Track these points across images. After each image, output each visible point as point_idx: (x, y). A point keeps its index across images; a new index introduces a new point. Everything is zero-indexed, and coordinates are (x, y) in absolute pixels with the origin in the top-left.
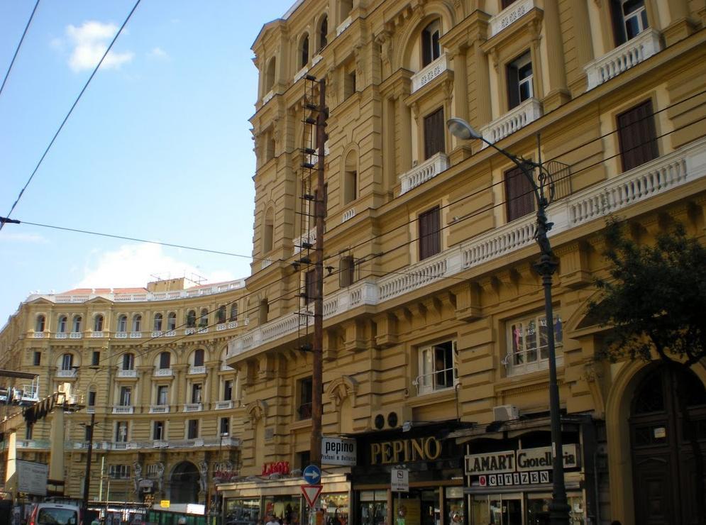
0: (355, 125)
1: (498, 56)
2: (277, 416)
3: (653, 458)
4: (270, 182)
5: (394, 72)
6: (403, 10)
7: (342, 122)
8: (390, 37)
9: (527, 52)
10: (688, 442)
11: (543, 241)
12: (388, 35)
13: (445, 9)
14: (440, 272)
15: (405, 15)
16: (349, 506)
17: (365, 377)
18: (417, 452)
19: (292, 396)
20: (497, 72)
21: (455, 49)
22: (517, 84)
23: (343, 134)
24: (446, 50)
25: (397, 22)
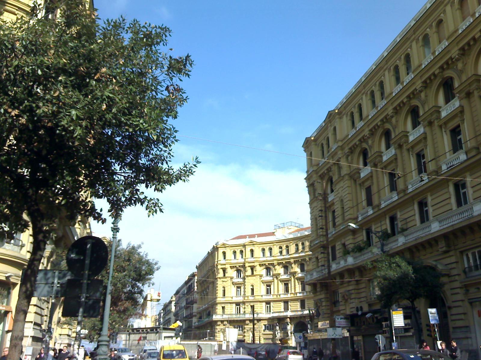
0: (342, 189)
1: (446, 126)
2: (325, 306)
5: (352, 170)
6: (465, 45)
9: (423, 150)
11: (329, 272)
13: (456, 75)
15: (432, 78)
16: (451, 330)
17: (353, 291)
20: (446, 134)
21: (463, 95)
22: (457, 138)
24: (458, 95)
25: (428, 81)
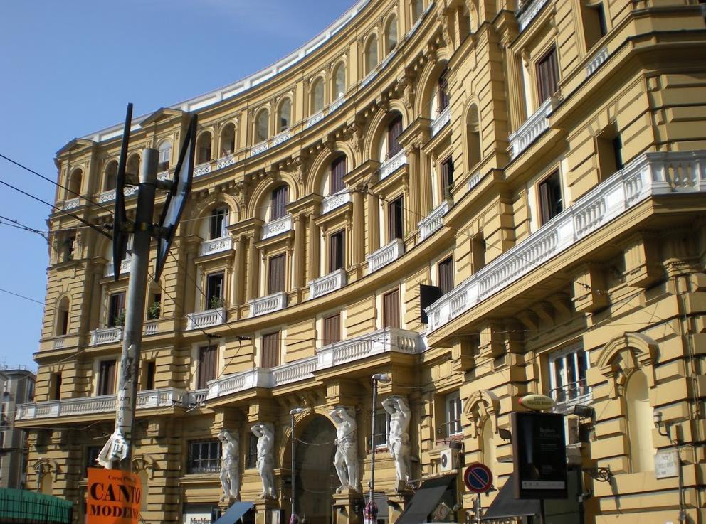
0: (472, 75)
3: (455, 404)
4: (469, 72)
7: (461, 73)
8: (412, 82)
10: (214, 436)
12: (410, 80)
14: (634, 193)
18: (110, 448)
19: (82, 459)
23: (462, 89)
